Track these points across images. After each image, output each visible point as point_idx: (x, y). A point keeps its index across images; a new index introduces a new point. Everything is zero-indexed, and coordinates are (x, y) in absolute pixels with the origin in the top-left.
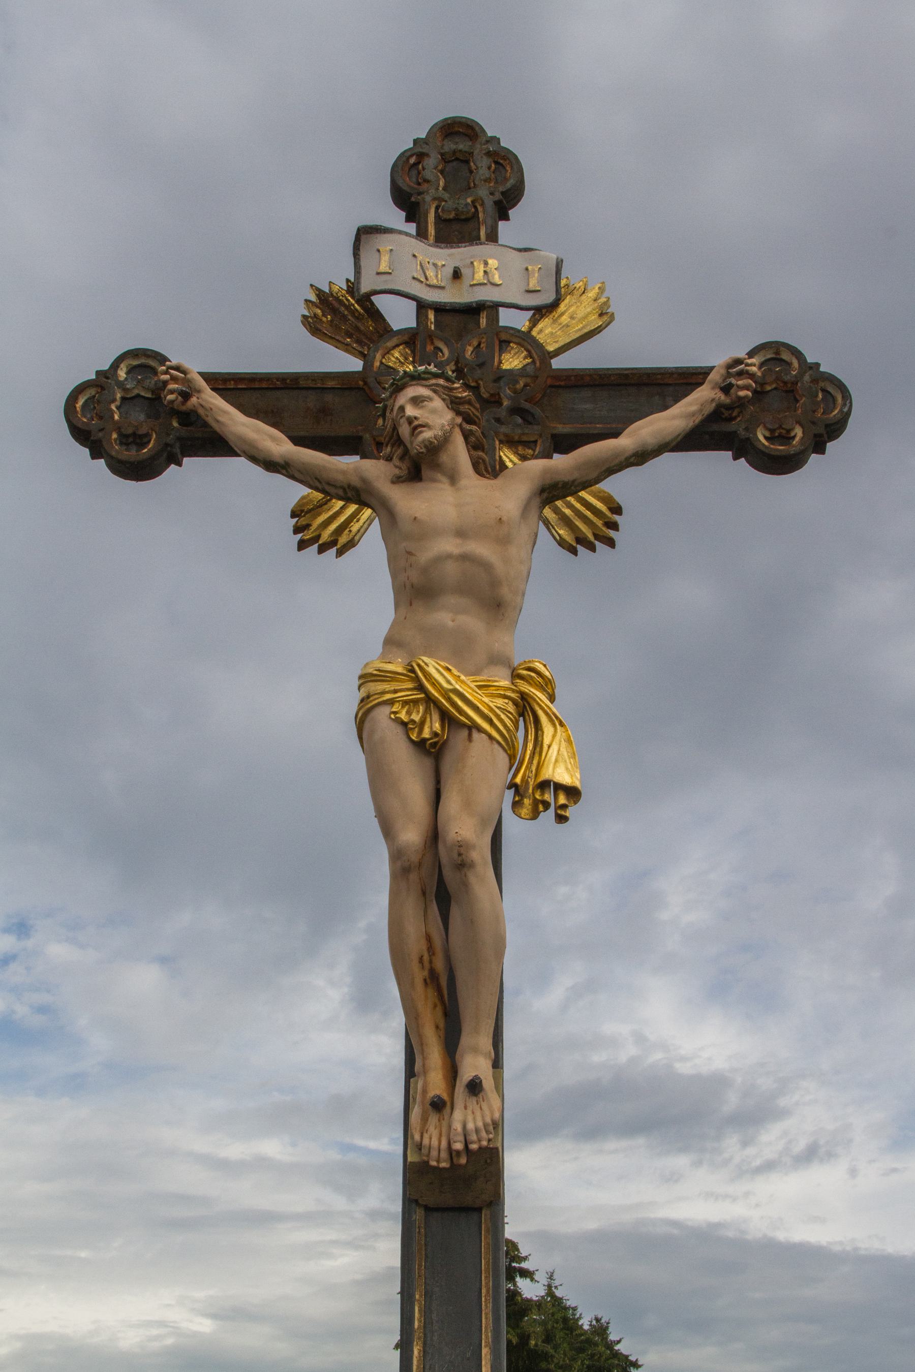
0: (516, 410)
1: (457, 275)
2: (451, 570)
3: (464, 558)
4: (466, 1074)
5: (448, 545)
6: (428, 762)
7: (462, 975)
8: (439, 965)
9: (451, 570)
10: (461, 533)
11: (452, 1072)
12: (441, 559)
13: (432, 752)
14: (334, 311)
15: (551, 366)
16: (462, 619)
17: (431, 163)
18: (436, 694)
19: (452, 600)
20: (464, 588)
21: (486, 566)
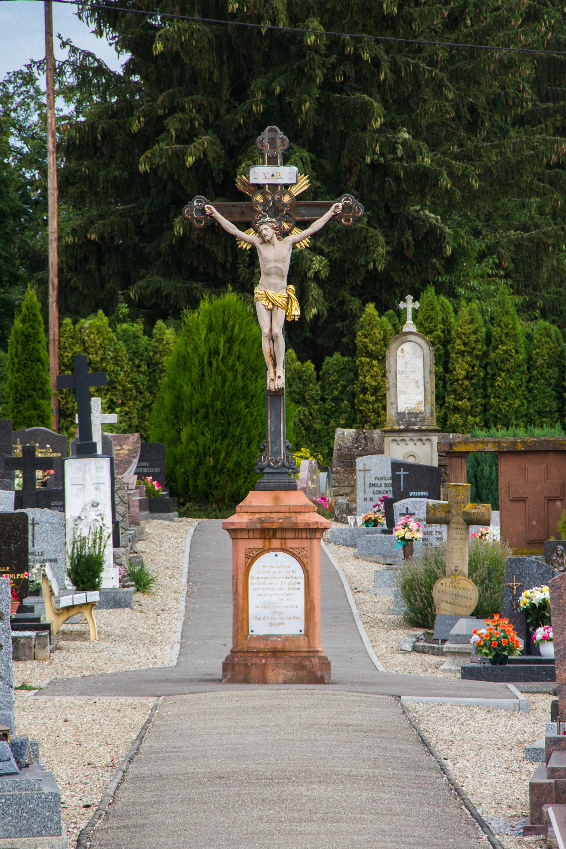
0: (287, 214)
1: (273, 175)
2: (273, 270)
3: (276, 267)
4: (278, 374)
5: (273, 264)
6: (269, 312)
7: (277, 355)
8: (272, 353)
9: (273, 270)
10: (275, 261)
11: (275, 373)
12: (271, 268)
13: (271, 310)
14: (244, 184)
15: (435, 468)
16: (276, 280)
17: (376, 72)
18: (269, 428)
19: (274, 276)
20: (276, 274)
21: (281, 269)
